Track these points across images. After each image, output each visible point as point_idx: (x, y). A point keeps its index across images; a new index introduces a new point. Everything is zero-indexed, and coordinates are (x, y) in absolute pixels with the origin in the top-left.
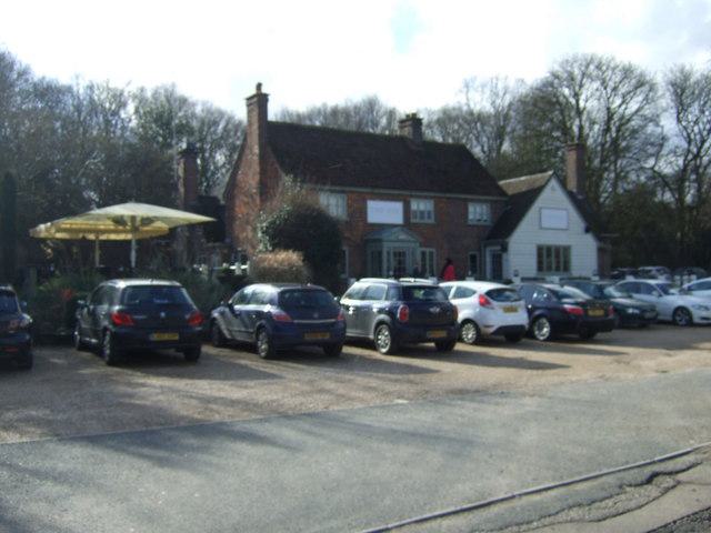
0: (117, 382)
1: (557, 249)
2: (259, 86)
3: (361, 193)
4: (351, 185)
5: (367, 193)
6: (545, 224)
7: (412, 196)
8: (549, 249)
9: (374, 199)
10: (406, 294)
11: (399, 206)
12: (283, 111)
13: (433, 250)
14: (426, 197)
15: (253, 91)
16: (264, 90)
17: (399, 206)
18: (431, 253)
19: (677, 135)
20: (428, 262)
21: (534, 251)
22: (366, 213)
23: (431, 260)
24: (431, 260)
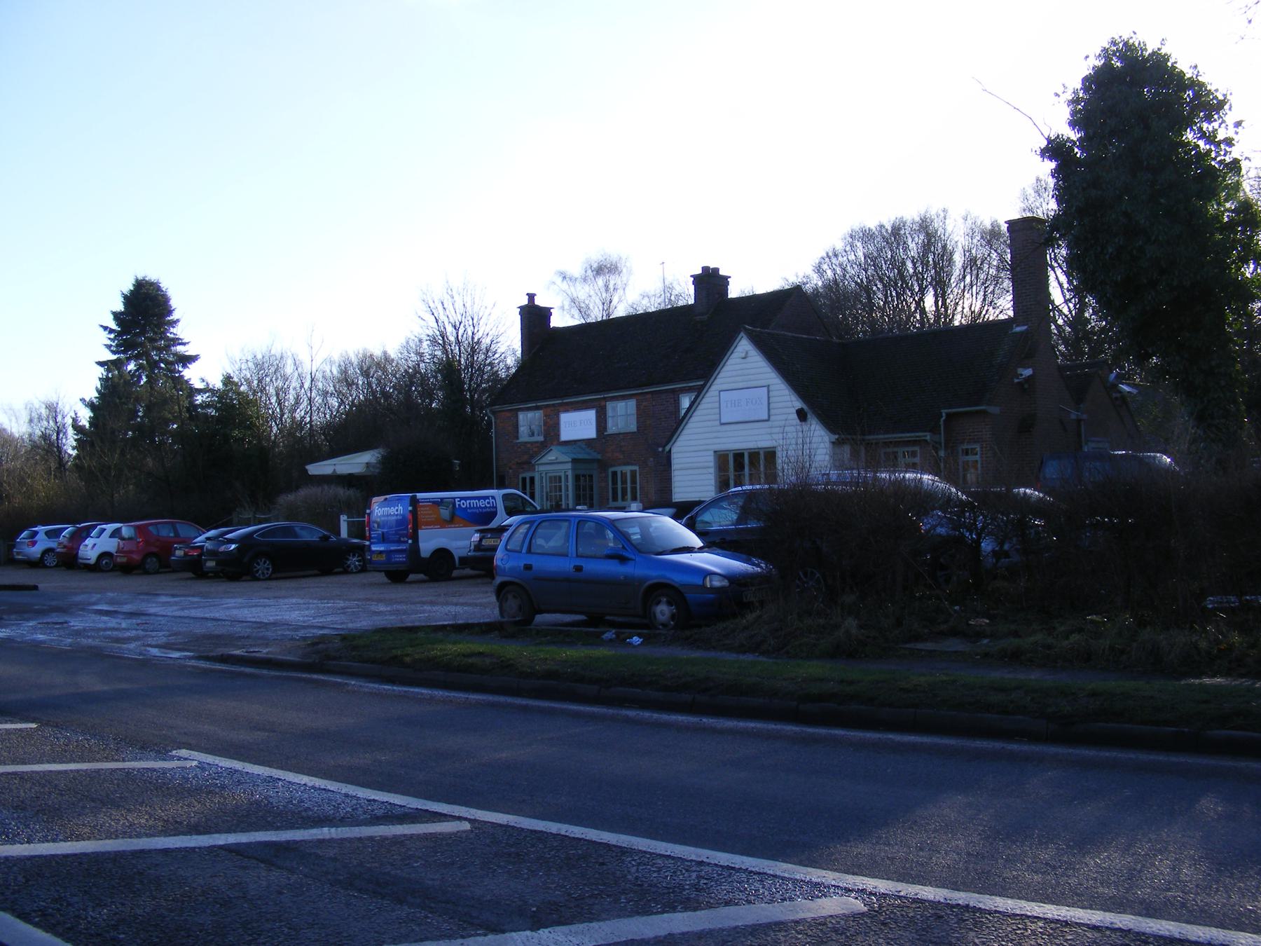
0: (82, 608)
1: (754, 455)
2: (531, 297)
3: (673, 391)
4: (545, 399)
5: (560, 405)
6: (766, 417)
7: (605, 399)
8: (739, 456)
9: (566, 411)
10: (138, 528)
11: (590, 415)
12: (440, 340)
13: (636, 468)
14: (624, 398)
15: (525, 301)
16: (539, 302)
17: (590, 415)
18: (633, 473)
19: (438, 359)
20: (619, 486)
21: (710, 460)
22: (559, 431)
23: (634, 482)
24: (634, 482)
